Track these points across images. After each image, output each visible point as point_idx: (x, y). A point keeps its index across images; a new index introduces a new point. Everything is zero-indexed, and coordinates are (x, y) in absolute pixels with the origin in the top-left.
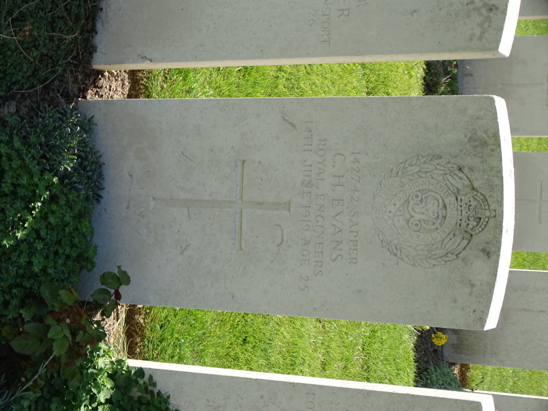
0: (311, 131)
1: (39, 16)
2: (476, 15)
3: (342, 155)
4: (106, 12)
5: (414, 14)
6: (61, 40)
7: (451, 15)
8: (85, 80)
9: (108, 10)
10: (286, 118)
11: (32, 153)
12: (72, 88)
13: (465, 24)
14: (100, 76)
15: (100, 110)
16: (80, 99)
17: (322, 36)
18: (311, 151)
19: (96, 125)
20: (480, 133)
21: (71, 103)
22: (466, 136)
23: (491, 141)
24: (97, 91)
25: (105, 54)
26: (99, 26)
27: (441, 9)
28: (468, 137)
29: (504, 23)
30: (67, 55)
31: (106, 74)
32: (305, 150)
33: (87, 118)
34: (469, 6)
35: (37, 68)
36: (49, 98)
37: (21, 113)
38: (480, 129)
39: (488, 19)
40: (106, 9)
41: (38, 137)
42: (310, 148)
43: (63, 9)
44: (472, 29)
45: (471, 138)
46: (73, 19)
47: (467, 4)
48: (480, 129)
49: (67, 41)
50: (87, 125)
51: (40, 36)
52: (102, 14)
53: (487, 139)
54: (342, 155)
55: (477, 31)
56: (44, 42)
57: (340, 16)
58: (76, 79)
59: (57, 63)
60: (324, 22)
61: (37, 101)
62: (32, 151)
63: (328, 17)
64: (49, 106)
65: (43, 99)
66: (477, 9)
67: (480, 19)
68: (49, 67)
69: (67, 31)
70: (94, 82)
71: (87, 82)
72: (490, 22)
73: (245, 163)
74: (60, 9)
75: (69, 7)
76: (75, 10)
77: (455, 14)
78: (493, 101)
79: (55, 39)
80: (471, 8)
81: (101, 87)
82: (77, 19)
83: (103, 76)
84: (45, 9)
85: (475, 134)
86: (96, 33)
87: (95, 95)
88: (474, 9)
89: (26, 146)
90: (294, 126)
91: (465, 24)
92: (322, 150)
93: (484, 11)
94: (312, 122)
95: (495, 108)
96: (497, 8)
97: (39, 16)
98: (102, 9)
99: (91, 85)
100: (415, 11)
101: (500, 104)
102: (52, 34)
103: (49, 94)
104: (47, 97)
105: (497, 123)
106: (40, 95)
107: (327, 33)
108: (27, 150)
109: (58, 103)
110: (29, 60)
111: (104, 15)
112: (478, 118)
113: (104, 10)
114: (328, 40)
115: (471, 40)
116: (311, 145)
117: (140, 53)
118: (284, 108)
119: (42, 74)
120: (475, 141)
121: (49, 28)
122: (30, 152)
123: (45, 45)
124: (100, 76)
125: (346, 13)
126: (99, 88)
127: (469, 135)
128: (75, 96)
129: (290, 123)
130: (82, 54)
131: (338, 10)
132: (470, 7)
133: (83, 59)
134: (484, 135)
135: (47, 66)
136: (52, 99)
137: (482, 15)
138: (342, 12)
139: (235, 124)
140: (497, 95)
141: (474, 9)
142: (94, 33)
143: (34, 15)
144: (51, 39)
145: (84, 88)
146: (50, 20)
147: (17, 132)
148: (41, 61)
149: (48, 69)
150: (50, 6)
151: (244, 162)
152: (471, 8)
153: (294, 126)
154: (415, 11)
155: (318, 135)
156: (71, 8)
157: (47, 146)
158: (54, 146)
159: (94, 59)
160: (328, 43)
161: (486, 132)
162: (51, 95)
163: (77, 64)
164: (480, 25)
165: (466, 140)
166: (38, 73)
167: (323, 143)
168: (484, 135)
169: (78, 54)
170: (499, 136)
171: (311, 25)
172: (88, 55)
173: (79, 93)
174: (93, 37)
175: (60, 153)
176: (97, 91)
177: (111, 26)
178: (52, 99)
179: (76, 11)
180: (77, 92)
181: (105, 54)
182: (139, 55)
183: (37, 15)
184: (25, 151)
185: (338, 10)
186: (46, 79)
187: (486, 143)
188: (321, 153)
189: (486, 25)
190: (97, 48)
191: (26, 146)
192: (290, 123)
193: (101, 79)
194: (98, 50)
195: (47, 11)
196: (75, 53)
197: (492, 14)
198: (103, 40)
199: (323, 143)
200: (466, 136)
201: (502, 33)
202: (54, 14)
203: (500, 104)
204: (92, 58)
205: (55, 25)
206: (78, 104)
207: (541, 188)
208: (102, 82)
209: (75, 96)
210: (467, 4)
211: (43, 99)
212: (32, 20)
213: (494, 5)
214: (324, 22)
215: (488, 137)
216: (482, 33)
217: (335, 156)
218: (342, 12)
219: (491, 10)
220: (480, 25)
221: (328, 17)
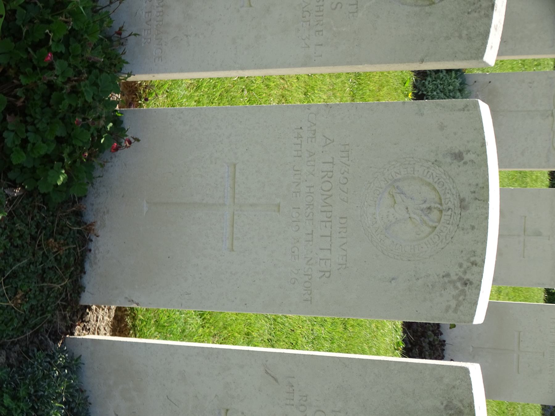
0: (293, 386)
1: (30, 271)
2: (451, 287)
3: (323, 412)
4: (95, 253)
5: (392, 282)
6: (50, 289)
7: (428, 286)
8: (73, 316)
9: (97, 252)
10: (269, 371)
11: (21, 407)
12: (60, 325)
13: (441, 295)
14: (87, 310)
15: (87, 348)
16: (68, 336)
17: (304, 295)
18: (293, 405)
19: (84, 364)
20: (456, 402)
21: (59, 340)
22: (442, 404)
23: (466, 411)
24: (84, 326)
25: (93, 294)
26: (87, 266)
27: (418, 279)
28: (444, 405)
29: (478, 298)
30: (57, 298)
31: (94, 307)
32: (287, 404)
33: (75, 358)
34: (445, 278)
35: (27, 318)
36: (38, 342)
37: (10, 361)
38: (455, 398)
39: (463, 292)
40: (95, 251)
41: (28, 388)
42: (292, 402)
43: (53, 259)
44: (448, 301)
45: (447, 406)
46: (63, 267)
47: (443, 277)
48: (455, 398)
49: (56, 288)
50: (74, 365)
51: (31, 290)
52: (91, 255)
53: (462, 408)
54: (323, 412)
55: (453, 303)
56: (34, 294)
57: (321, 277)
58: (65, 317)
59: (47, 309)
60: (306, 282)
61: (26, 344)
62: (22, 404)
63: (310, 277)
64: (38, 350)
65: (32, 342)
66: (452, 282)
67: (455, 292)
68: (39, 314)
69: (57, 279)
70: (82, 318)
71: (75, 318)
72: (465, 295)
73: (229, 412)
74: (50, 261)
75: (59, 257)
76: (64, 260)
77: (431, 285)
78: (478, 101)
79: (45, 289)
80: (447, 281)
81: (88, 322)
82: (67, 267)
83: (90, 309)
84: (36, 263)
85: (451, 402)
86: (85, 273)
87: (83, 330)
88: (450, 282)
89: (16, 401)
90: (276, 380)
91: (441, 295)
92: (304, 405)
93: (459, 284)
94: (294, 377)
95: (470, 379)
96: (471, 283)
97: (30, 271)
98: (90, 250)
99: (79, 320)
100: (393, 279)
101: (484, 109)
102: (42, 285)
103: (38, 337)
104: (35, 340)
105: (472, 393)
106: (29, 338)
107: (309, 292)
108: (16, 405)
109: (46, 346)
110: (19, 313)
111: (92, 256)
112: (454, 387)
113: (92, 251)
114: (310, 299)
115: (447, 310)
116: (293, 400)
117: (127, 296)
118: (267, 361)
119: (32, 322)
120: (451, 409)
121: (39, 280)
122: (19, 407)
123: (35, 297)
124: (87, 310)
125: (327, 274)
126: (86, 322)
127: (445, 403)
128: (62, 333)
129: (273, 377)
130: (71, 295)
131: (320, 271)
132: (446, 279)
133: (71, 300)
134: (460, 405)
135: (37, 314)
136: (41, 342)
137: (457, 288)
138: (323, 273)
139: (219, 373)
140: (483, 101)
141: (450, 282)
142: (82, 274)
143: (25, 271)
144: (41, 290)
145: (72, 324)
146: (40, 272)
147: (7, 385)
148: (31, 312)
149: (38, 316)
150: (41, 259)
151: (227, 410)
152: (447, 281)
153: (276, 380)
154: (393, 279)
155: (300, 391)
156: (61, 258)
157: (36, 396)
158: (42, 396)
159: (82, 298)
160: (309, 302)
161: (461, 401)
162: (40, 337)
163: (65, 305)
164: (455, 297)
165: (442, 407)
166: (28, 322)
167: (304, 399)
168: (460, 405)
169: (67, 295)
170: (474, 407)
171: (294, 284)
172: (76, 295)
173: (67, 330)
174: (81, 278)
175: (48, 402)
176: (84, 326)
177: (99, 267)
178: (41, 342)
179: (66, 260)
180: (64, 329)
181: (93, 294)
182: (126, 298)
183: (28, 271)
184: (14, 407)
185: (320, 271)
186: (36, 325)
187: (469, 157)
188: (302, 408)
189: (461, 298)
190: (85, 288)
191: (16, 401)
192: (273, 377)
193: (88, 314)
194: (86, 290)
195: (38, 264)
196: (63, 296)
197: (466, 288)
198: (92, 280)
199: (304, 399)
200: (442, 404)
201: (476, 307)
202: (44, 265)
203: (484, 109)
204: (80, 297)
205: (45, 276)
206: (66, 340)
207: (519, 338)
208: (91, 316)
209: (62, 333)
210: (443, 277)
211: (32, 342)
212: (23, 277)
213: (468, 280)
214: (306, 282)
215: (463, 407)
216: (458, 305)
217: (315, 412)
218: (323, 273)
219: (466, 284)
220: (455, 297)
221: (310, 277)
